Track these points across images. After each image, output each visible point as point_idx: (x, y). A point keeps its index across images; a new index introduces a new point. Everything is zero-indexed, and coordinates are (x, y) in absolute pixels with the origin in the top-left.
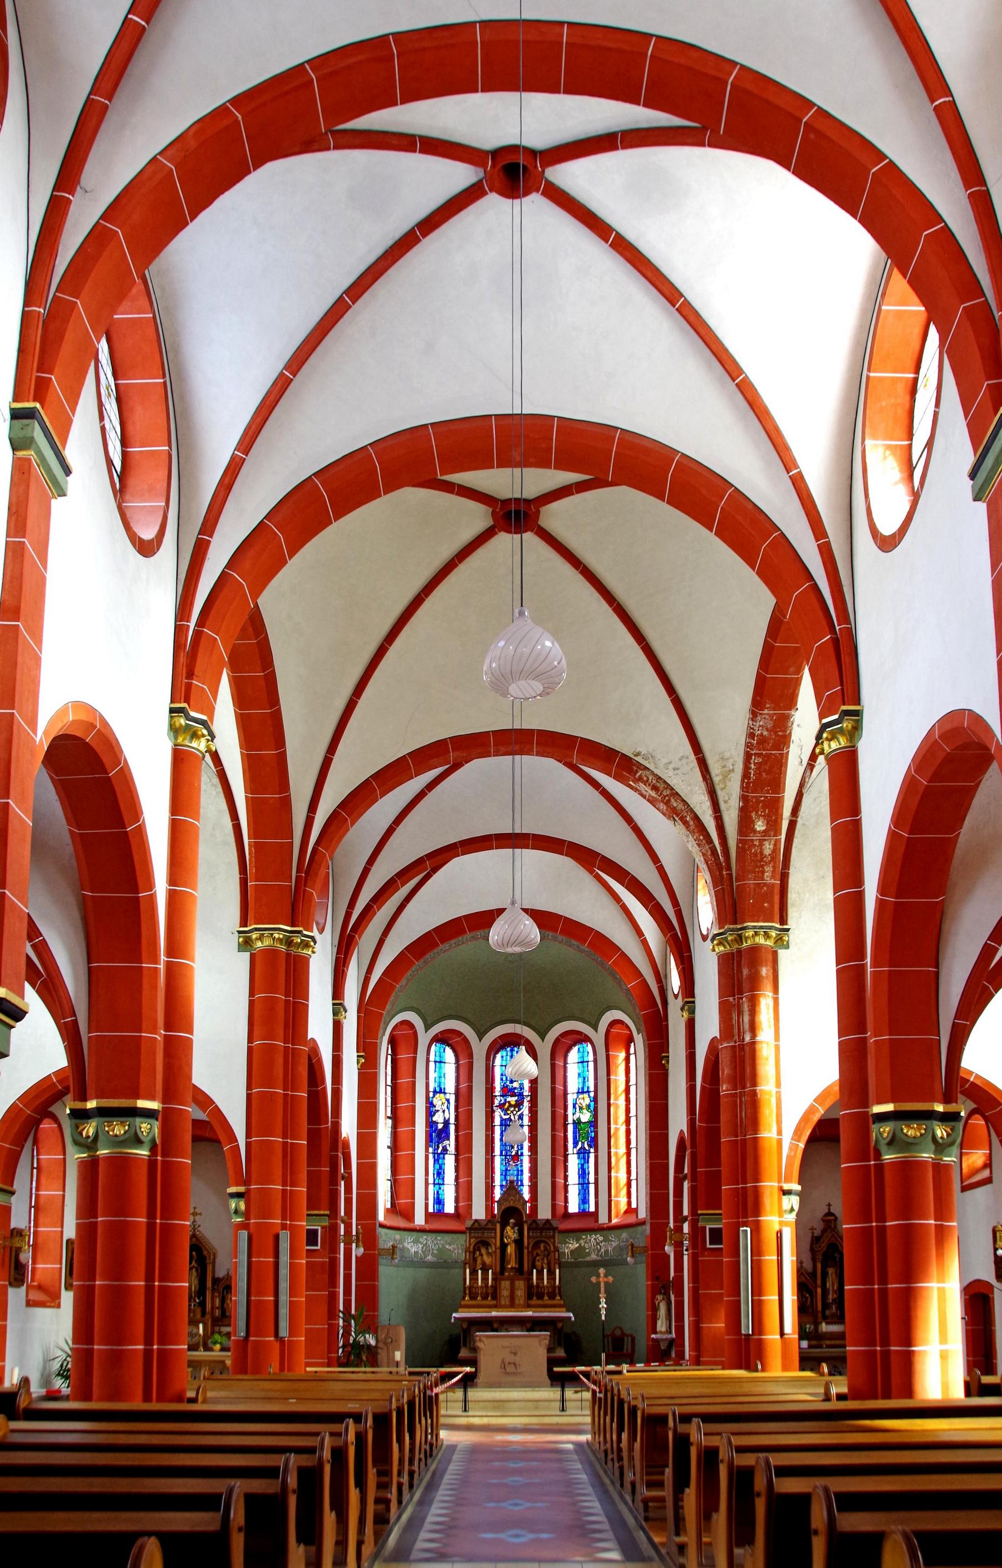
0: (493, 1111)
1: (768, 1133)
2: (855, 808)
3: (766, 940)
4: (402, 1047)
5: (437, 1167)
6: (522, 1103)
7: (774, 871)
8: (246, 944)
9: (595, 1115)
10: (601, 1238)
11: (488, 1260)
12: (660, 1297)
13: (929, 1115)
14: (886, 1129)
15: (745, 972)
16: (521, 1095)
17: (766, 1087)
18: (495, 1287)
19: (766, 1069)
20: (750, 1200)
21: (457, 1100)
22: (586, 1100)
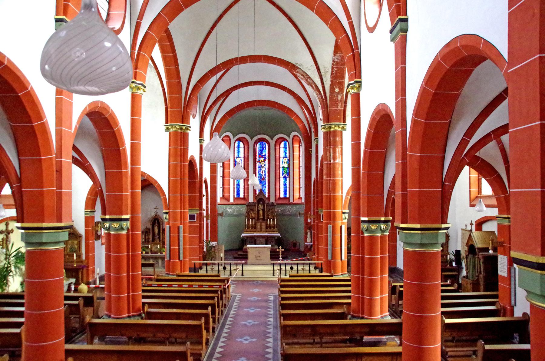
1: (339, 194)
2: (359, 114)
8: (167, 129)
9: (289, 164)
11: (253, 215)
12: (308, 230)
13: (379, 222)
14: (365, 226)
15: (331, 139)
16: (265, 158)
18: (255, 224)
20: (332, 215)
22: (286, 160)
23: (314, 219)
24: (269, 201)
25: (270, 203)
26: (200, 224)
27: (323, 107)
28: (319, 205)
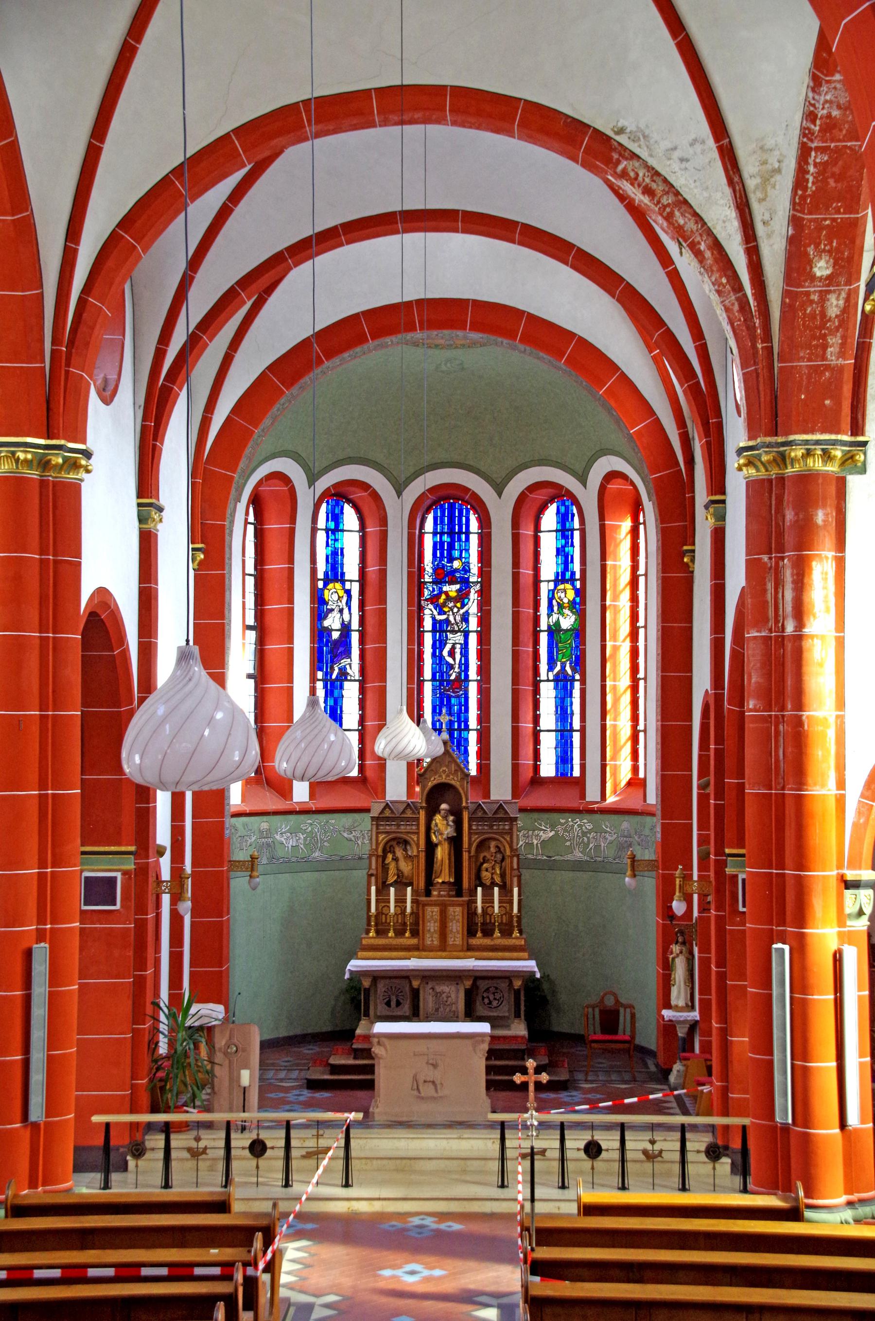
0: (421, 609)
1: (822, 787)
3: (825, 462)
4: (271, 510)
5: (331, 702)
6: (467, 595)
7: (843, 345)
9: (581, 615)
10: (589, 826)
11: (406, 867)
12: (676, 948)
15: (789, 515)
16: (465, 582)
17: (820, 711)
18: (415, 914)
19: (820, 680)
21: (362, 592)
23: (702, 897)
24: (487, 795)
25: (489, 810)
26: (141, 926)
27: (747, 358)
28: (729, 834)
